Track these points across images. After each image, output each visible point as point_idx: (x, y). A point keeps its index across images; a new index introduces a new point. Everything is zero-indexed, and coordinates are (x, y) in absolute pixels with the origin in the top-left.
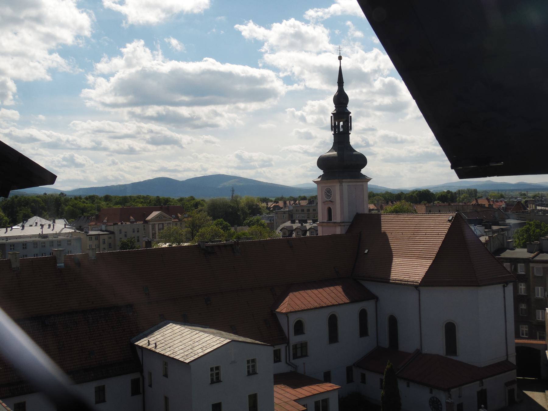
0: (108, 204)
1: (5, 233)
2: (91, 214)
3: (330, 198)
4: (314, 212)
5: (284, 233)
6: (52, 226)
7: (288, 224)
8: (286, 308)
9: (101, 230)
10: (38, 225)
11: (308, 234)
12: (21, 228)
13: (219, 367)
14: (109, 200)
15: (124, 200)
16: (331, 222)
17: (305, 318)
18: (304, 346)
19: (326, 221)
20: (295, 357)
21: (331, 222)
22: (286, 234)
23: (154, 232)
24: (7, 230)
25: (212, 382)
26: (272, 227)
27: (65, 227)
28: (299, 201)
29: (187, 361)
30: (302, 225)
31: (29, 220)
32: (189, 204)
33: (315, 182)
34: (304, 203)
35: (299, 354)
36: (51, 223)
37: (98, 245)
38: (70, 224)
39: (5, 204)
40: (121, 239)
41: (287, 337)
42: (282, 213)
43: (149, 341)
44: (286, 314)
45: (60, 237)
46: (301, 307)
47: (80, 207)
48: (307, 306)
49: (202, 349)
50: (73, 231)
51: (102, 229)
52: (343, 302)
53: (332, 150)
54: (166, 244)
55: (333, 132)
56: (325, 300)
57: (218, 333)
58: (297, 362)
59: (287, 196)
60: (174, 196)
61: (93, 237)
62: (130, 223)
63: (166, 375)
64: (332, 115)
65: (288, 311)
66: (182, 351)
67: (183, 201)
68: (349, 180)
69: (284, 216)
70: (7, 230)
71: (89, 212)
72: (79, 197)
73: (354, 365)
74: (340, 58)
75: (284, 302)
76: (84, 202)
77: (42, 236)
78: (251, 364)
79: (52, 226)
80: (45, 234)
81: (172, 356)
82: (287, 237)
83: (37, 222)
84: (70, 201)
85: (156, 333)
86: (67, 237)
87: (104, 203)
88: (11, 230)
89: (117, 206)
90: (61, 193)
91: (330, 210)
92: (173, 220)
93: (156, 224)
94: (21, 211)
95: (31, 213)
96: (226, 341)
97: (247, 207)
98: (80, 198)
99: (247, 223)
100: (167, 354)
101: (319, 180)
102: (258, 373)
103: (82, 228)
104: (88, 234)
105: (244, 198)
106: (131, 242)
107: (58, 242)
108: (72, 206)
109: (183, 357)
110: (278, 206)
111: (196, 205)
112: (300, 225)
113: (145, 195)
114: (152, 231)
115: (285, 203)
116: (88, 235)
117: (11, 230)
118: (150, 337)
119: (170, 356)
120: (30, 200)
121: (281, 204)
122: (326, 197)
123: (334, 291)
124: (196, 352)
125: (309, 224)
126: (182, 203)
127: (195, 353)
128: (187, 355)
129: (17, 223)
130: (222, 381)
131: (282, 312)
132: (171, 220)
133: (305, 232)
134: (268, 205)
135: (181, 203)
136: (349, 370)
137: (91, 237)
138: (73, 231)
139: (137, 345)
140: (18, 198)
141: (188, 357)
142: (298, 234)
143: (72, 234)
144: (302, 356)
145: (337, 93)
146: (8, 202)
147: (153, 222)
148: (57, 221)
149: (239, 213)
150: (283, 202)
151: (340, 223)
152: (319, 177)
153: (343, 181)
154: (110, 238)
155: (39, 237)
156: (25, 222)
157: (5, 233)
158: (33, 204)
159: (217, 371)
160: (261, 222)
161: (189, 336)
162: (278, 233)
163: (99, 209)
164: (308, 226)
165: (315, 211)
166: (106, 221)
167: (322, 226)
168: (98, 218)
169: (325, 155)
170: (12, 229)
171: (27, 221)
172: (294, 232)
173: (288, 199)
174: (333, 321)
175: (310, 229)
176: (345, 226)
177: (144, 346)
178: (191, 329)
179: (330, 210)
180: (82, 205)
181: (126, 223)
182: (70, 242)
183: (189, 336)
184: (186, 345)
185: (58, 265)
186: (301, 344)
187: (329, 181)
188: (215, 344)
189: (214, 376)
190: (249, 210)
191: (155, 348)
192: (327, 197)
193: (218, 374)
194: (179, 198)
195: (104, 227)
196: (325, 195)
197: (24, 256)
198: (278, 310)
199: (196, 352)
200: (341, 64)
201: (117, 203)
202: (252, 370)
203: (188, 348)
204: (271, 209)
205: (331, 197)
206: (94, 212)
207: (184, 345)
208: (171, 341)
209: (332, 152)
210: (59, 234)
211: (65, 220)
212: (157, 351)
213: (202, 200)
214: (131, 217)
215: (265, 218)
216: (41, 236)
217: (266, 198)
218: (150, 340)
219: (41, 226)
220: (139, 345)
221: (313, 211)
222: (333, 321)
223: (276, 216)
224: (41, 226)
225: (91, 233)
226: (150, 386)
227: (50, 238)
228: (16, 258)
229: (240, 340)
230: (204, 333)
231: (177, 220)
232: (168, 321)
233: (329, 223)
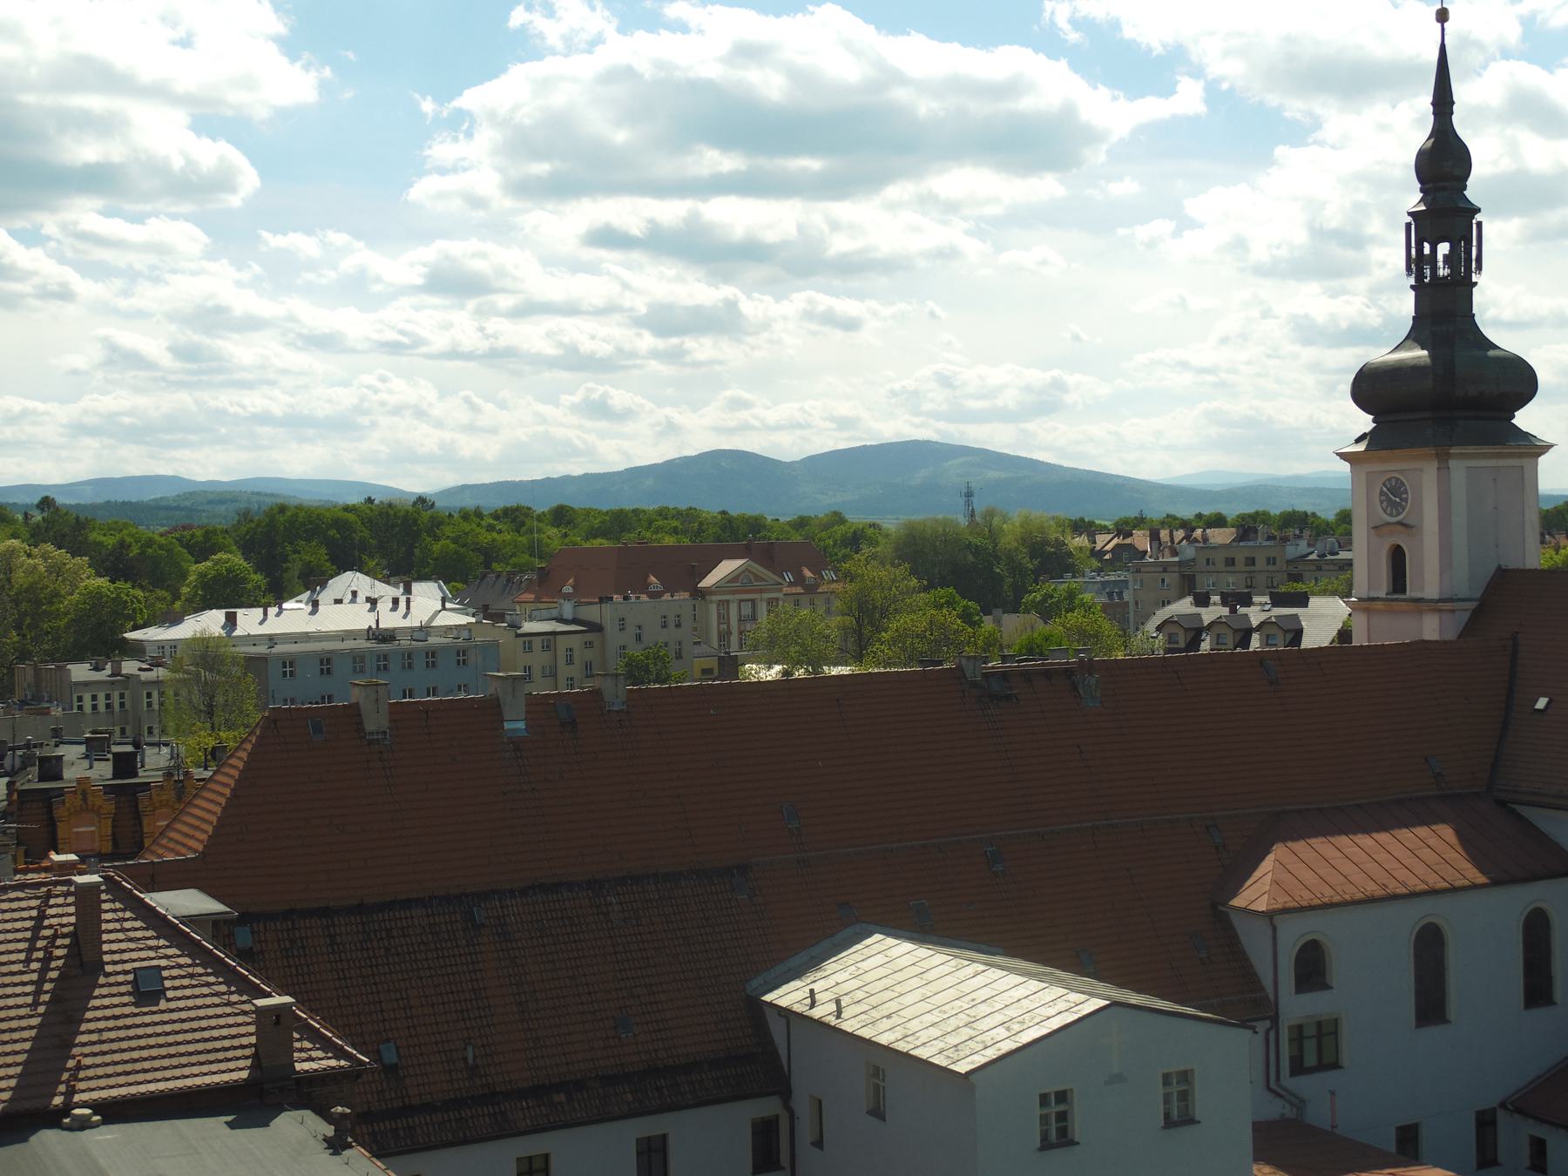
0: (566, 535)
1: (261, 623)
2: (515, 566)
3: (1398, 514)
4: (1271, 568)
5: (1171, 638)
6: (402, 604)
7: (1184, 606)
8: (1266, 896)
9: (560, 620)
10: (358, 599)
11: (1255, 643)
12: (310, 608)
13: (1068, 1092)
14: (569, 523)
15: (620, 522)
16: (1404, 597)
17: (1332, 931)
18: (1326, 1032)
19: (1382, 594)
20: (1298, 1068)
21: (1404, 597)
22: (1178, 643)
23: (725, 626)
24: (265, 614)
25: (1046, 1145)
26: (1122, 615)
27: (444, 608)
28: (1204, 530)
29: (962, 1068)
30: (1233, 611)
31: (330, 582)
32: (829, 538)
33: (1344, 456)
34: (1221, 536)
35: (1310, 1060)
36: (398, 592)
37: (550, 667)
38: (457, 595)
39: (247, 533)
40: (624, 647)
41: (1271, 996)
42: (1158, 569)
43: (812, 991)
44: (1270, 915)
45: (432, 640)
46: (1319, 895)
47: (478, 543)
48: (1341, 893)
49: (1008, 1029)
50: (473, 620)
51: (562, 616)
52: (1466, 883)
53: (1409, 342)
54: (770, 668)
55: (1412, 281)
56: (1402, 874)
57: (1043, 974)
58: (1306, 1085)
59: (1156, 512)
60: (779, 510)
61: (537, 642)
62: (648, 596)
63: (877, 1112)
64: (1409, 219)
65: (1276, 906)
66: (935, 1032)
67: (807, 527)
68: (1470, 450)
69: (1163, 580)
70: (265, 614)
71: (511, 561)
72: (476, 511)
73: (1503, 1105)
74: (1442, 16)
75: (1257, 874)
76: (490, 528)
77: (377, 634)
78: (1175, 1089)
79: (402, 604)
80: (386, 630)
81: (902, 1046)
82: (1180, 651)
83: (355, 589)
84: (449, 524)
85: (831, 966)
86: (454, 638)
87: (553, 531)
88: (278, 615)
89: (594, 542)
90: (420, 497)
91: (1397, 555)
92: (786, 590)
93: (733, 602)
94: (294, 556)
95: (326, 561)
96: (1089, 1002)
97: (1024, 550)
98: (478, 513)
99: (1033, 601)
100: (884, 1040)
101: (1361, 447)
102: (1199, 1122)
103: (489, 611)
104: (519, 631)
105: (1015, 516)
106: (657, 658)
107: (427, 654)
108: (455, 541)
109: (945, 1053)
110: (1131, 546)
111: (855, 540)
112: (1225, 611)
113: (683, 506)
114: (719, 623)
115: (1155, 536)
116: (518, 636)
117: (278, 615)
118: (812, 978)
119: (895, 1046)
120: (325, 520)
121: (1141, 540)
122: (1385, 511)
123: (1432, 841)
124: (987, 1038)
125: (1259, 607)
126: (803, 533)
127: (983, 1042)
128: (956, 1046)
129: (285, 595)
130: (1078, 1143)
131: (1252, 907)
132: (780, 590)
133: (1245, 635)
134: (1095, 542)
135: (800, 535)
136: (1485, 1123)
137: (530, 642)
138: (473, 620)
139: (770, 1004)
140: (289, 514)
141: (962, 1054)
142: (1220, 641)
143: (470, 630)
144: (1322, 1067)
145: (1432, 140)
146: (258, 526)
147: (720, 594)
148: (416, 587)
149: (998, 570)
150: (1148, 533)
151: (1440, 601)
152: (1358, 441)
153: (1451, 451)
154: (588, 645)
155: (368, 639)
156: (318, 588)
157: (261, 623)
158: (332, 532)
159: (1062, 1108)
160: (1082, 599)
161: (950, 980)
162: (1149, 638)
163: (536, 549)
164: (1255, 615)
165: (1274, 563)
166: (571, 590)
167: (1367, 611)
168: (546, 583)
169: (1381, 363)
170: (281, 610)
171: (324, 585)
172: (1204, 635)
173: (1163, 523)
174: (1430, 944)
175: (1262, 624)
176: (1457, 612)
177: (798, 1008)
178: (956, 957)
179: (1397, 555)
180: (486, 538)
181: (638, 598)
182: (385, 659)
183: (950, 980)
184: (945, 1012)
185: (507, 726)
186: (1319, 1024)
187: (1397, 452)
188: (1052, 1011)
189: (1051, 1125)
190: (1031, 558)
191: (838, 1017)
192: (1388, 512)
193: (1062, 1116)
194: (795, 517)
195: (568, 610)
196: (1382, 502)
197: (323, 698)
198: (1237, 902)
199: (989, 1038)
200: (1446, 37)
201: (593, 534)
202: (1178, 1107)
203: (953, 1022)
204: (1107, 557)
205: (1404, 510)
206: (525, 558)
207: (940, 1012)
208: (889, 994)
209: (1410, 349)
210: (425, 630)
211: (442, 584)
212: (847, 1026)
213: (870, 526)
214: (652, 579)
215: (1091, 586)
216: (373, 634)
217: (1082, 520)
218: (817, 987)
219: (369, 604)
220: (776, 1005)
221: (1268, 563)
222: (1430, 944)
223: (1136, 580)
224: (369, 604)
225: (529, 627)
226: (819, 1144)
227: (405, 643)
228: (377, 700)
229: (1133, 1002)
230: (1005, 973)
231: (799, 590)
232: (864, 925)
233: (1396, 600)
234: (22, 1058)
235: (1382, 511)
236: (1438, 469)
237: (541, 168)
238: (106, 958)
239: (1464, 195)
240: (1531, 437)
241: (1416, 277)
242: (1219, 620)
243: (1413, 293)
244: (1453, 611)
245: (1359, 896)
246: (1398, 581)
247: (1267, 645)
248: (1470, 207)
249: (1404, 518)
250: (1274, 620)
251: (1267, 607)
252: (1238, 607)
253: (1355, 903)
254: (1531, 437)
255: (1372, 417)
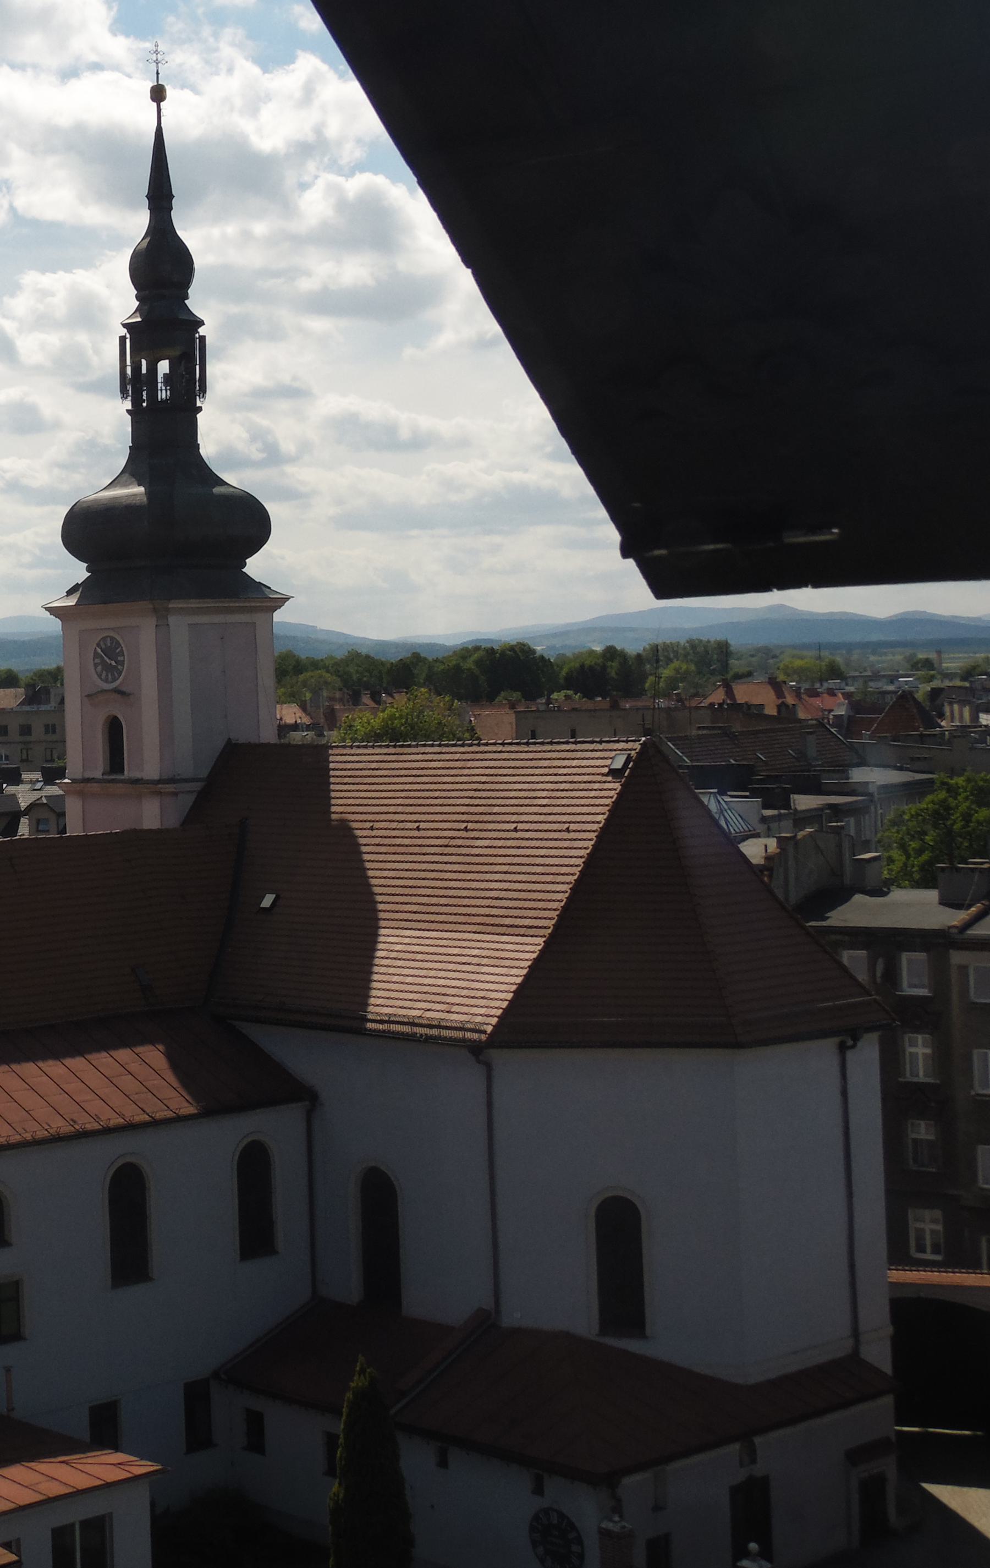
3: (114, 680)
11: (24, 829)
19: (98, 774)
21: (122, 777)
48: (21, 1131)
52: (169, 1114)
55: (128, 405)
56: (96, 1106)
64: (124, 332)
73: (216, 1375)
74: (158, 94)
91: (114, 729)
101: (72, 602)
122: (100, 676)
123: (135, 1067)
125: (28, 786)
145: (148, 240)
151: (159, 781)
152: (70, 593)
153: (170, 606)
165: (54, 732)
167: (81, 794)
169: (95, 501)
179: (114, 729)
192: (103, 677)
196: (96, 665)
200: (163, 119)
209: (125, 485)
221: (47, 732)
234: (608, 801)
235: (96, 676)
236: (156, 626)
237: (945, 902)
238: (364, 849)
239: (185, 304)
240: (264, 588)
241: (132, 401)
242: (38, 802)
243: (129, 417)
244: (175, 794)
245: (41, 1134)
246: (116, 761)
247: (38, 831)
248: (192, 319)
249: (121, 684)
250: (45, 801)
251: (39, 786)
252: (5, 785)
253: (36, 1143)
254: (264, 588)
255: (86, 565)
